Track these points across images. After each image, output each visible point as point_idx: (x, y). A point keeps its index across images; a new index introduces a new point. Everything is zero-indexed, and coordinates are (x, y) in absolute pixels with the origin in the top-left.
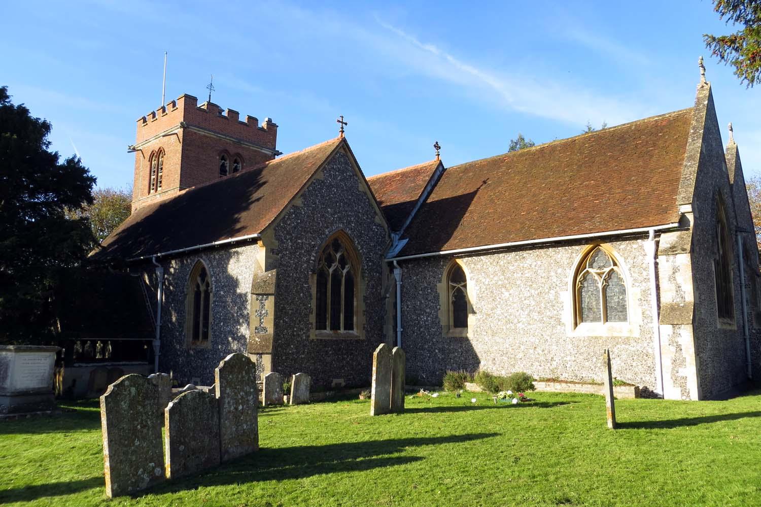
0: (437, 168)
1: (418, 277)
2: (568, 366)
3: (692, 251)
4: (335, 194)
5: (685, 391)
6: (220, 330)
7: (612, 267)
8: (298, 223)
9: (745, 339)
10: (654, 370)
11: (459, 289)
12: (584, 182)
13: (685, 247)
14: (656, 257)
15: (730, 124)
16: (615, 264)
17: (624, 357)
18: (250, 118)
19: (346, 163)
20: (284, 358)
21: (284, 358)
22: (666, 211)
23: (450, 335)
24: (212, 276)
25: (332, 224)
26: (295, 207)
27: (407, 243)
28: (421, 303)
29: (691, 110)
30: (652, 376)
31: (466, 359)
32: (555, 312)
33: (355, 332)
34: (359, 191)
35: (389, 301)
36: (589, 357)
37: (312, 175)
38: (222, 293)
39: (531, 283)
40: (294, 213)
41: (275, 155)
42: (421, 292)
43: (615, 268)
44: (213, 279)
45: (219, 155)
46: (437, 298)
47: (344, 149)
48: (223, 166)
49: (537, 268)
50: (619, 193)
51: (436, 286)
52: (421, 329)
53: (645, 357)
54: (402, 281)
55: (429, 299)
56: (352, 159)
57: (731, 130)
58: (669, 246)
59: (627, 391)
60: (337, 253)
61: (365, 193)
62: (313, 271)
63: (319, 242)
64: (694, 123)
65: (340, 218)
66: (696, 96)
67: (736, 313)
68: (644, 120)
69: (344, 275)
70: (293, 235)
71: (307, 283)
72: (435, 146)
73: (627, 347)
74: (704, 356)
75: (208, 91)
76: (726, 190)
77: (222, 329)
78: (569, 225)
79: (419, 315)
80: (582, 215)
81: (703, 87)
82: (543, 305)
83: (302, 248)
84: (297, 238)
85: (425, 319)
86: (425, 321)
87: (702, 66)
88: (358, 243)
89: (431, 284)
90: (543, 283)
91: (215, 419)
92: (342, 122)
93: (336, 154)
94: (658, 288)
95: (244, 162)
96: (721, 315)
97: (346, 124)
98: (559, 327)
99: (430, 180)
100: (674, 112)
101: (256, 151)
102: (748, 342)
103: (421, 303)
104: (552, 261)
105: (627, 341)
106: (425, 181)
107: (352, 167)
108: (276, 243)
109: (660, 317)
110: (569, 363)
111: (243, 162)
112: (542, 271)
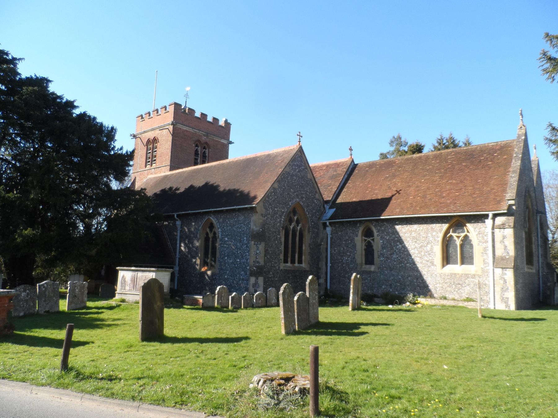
0: (351, 164)
1: (342, 233)
2: (438, 290)
3: (514, 227)
4: (295, 180)
5: (507, 306)
6: (225, 262)
7: (466, 233)
8: (275, 198)
9: (539, 278)
10: (489, 294)
11: (369, 242)
12: (449, 180)
13: (510, 224)
14: (493, 228)
15: (534, 145)
16: (468, 232)
17: (472, 286)
18: (202, 114)
19: (301, 161)
20: (267, 280)
21: (267, 280)
22: (499, 202)
23: (363, 269)
24: (218, 229)
25: (293, 199)
26: (274, 188)
27: (335, 212)
28: (344, 249)
29: (514, 140)
30: (488, 297)
31: (373, 284)
32: (431, 258)
33: (303, 265)
34: (308, 179)
35: (323, 247)
36: (451, 285)
37: (284, 169)
38: (226, 239)
39: (416, 240)
40: (273, 192)
41: (229, 143)
42: (344, 242)
43: (468, 234)
44: (219, 230)
45: (194, 144)
46: (354, 246)
47: (301, 152)
48: (197, 151)
49: (420, 231)
50: (471, 189)
51: (354, 239)
52: (344, 265)
53: (484, 286)
54: (331, 235)
55: (349, 247)
56: (305, 158)
57: (535, 149)
58: (501, 223)
59: (474, 305)
60: (295, 216)
61: (311, 180)
62: (283, 227)
63: (286, 210)
64: (516, 150)
65: (297, 195)
66: (517, 133)
67: (535, 262)
68: (485, 144)
69: (291, 229)
70: (273, 205)
71: (279, 235)
72: (350, 149)
73: (474, 280)
74: (518, 286)
75: (185, 98)
76: (532, 189)
77: (226, 261)
78: (441, 207)
79: (342, 256)
80: (449, 202)
81: (521, 127)
82: (423, 253)
83: (277, 213)
84: (275, 207)
85: (347, 259)
86: (346, 260)
87: (521, 114)
88: (307, 211)
89: (351, 238)
90: (423, 240)
91: (307, 306)
92: (300, 136)
93: (296, 156)
94: (494, 247)
95: (210, 148)
96: (527, 264)
97: (302, 137)
98: (432, 267)
99: (347, 172)
100: (504, 141)
101: (218, 141)
102: (541, 279)
103: (344, 249)
104: (429, 228)
105: (474, 276)
106: (343, 171)
107: (305, 163)
108: (264, 210)
109: (495, 263)
110: (439, 288)
111: (209, 148)
112: (423, 233)
